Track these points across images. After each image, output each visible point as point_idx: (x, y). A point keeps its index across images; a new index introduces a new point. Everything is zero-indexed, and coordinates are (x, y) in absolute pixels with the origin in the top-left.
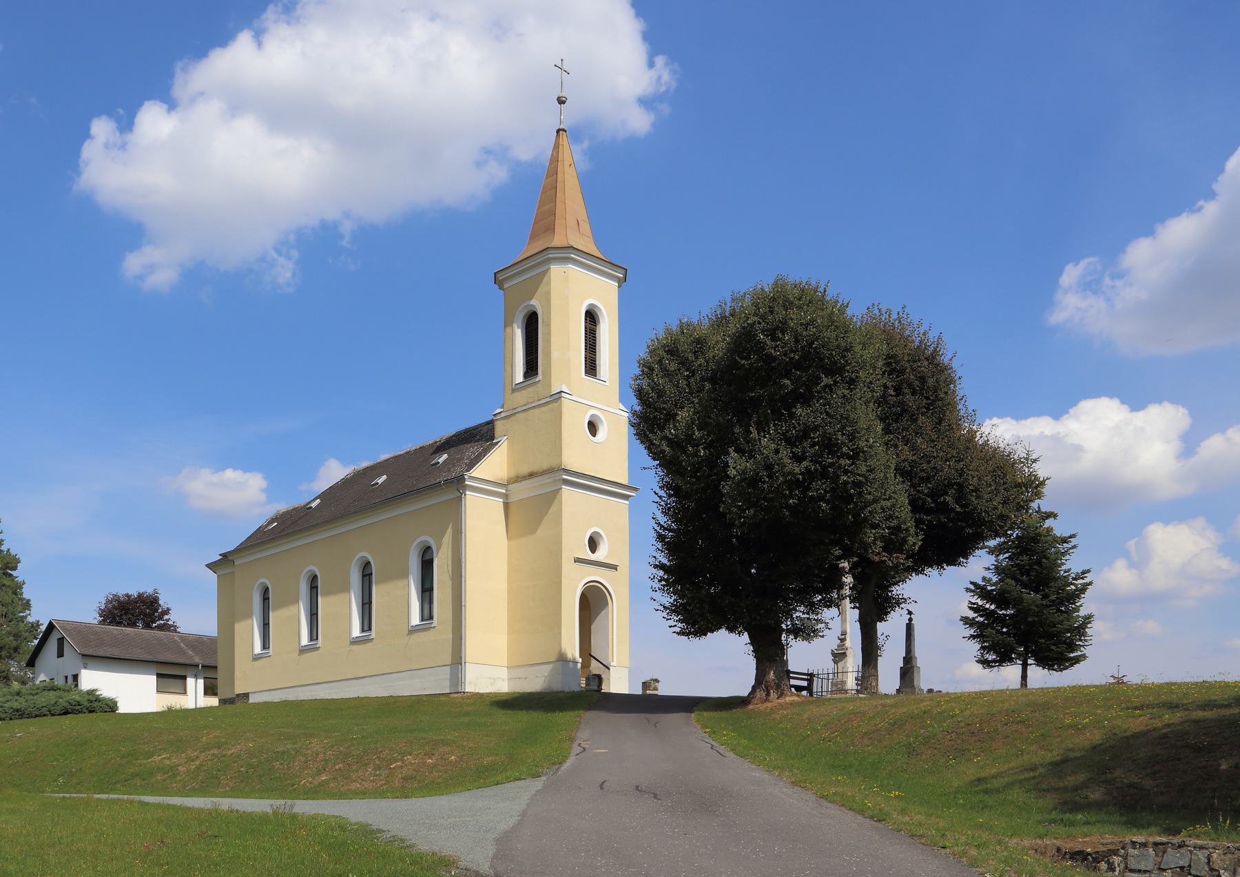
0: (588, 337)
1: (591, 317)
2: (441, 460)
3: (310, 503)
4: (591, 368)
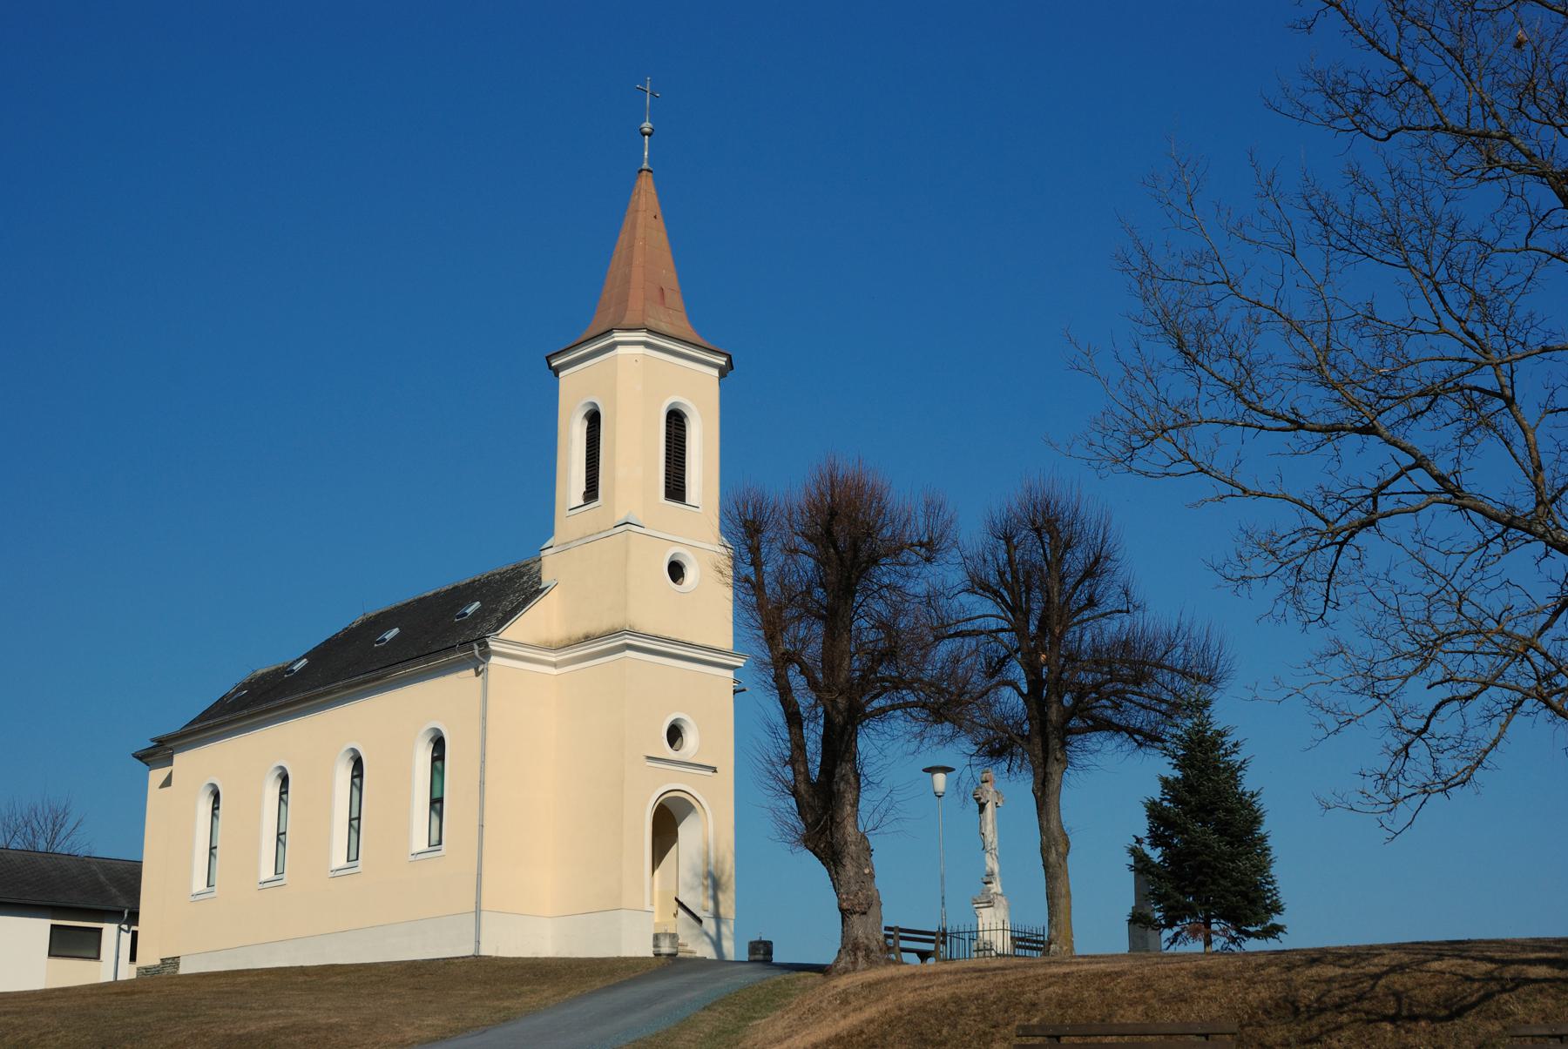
1: (676, 420)
2: (470, 610)
3: (293, 664)
4: (675, 489)
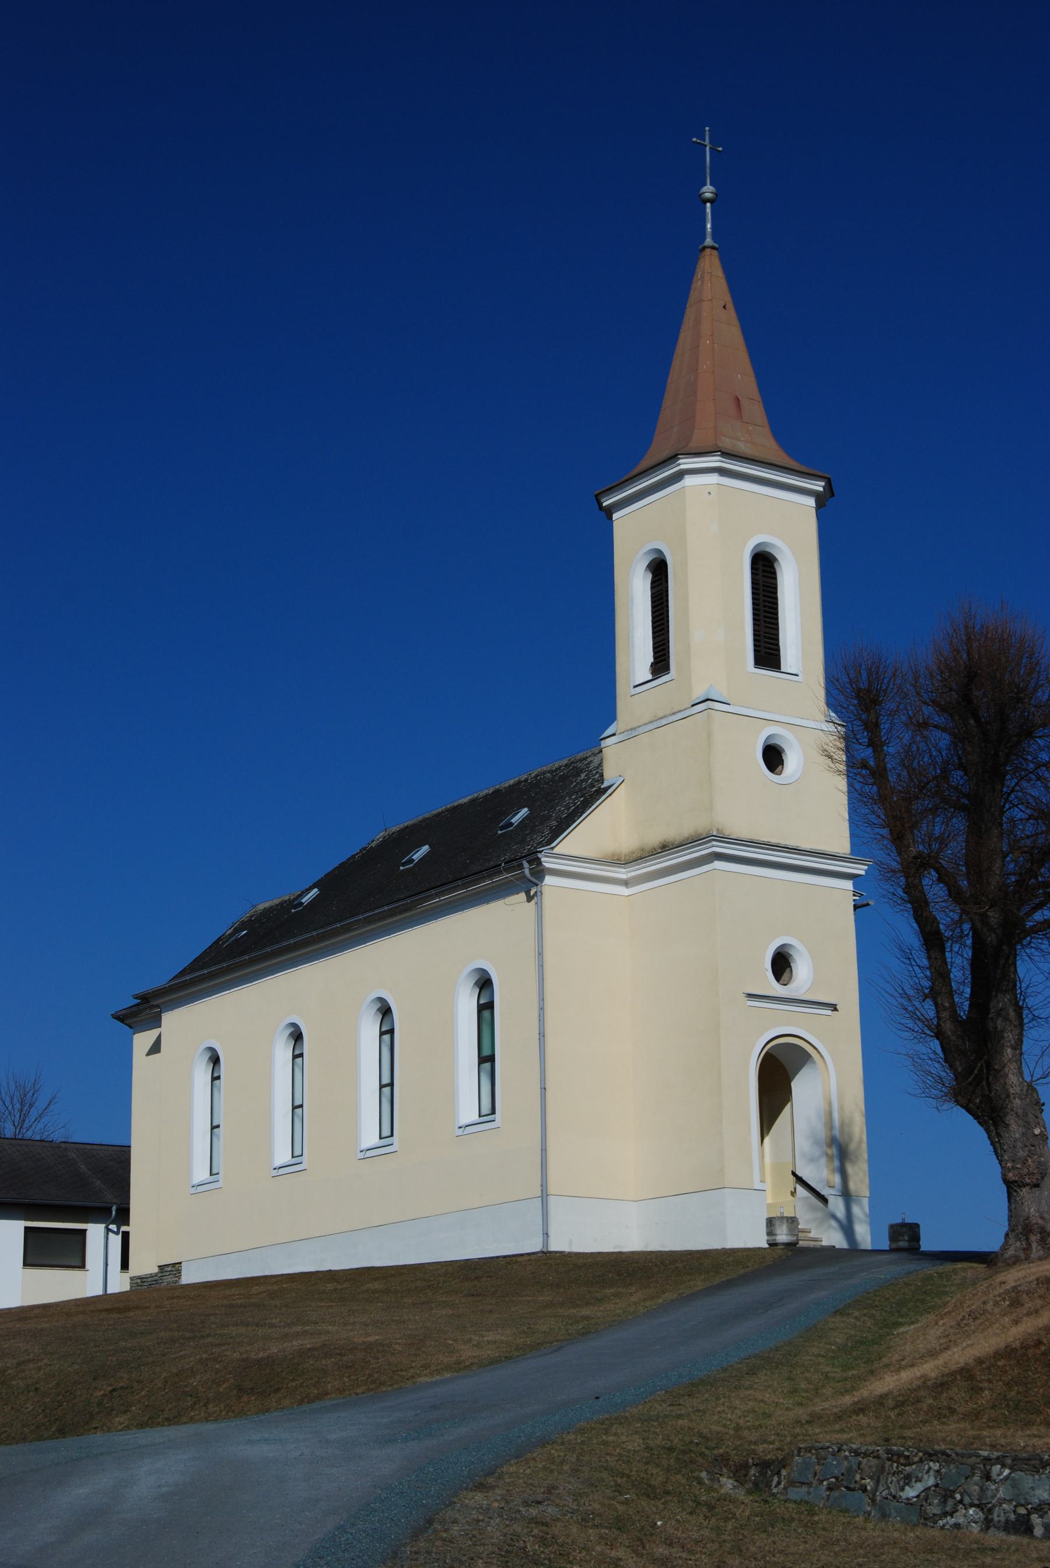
0: (762, 598)
